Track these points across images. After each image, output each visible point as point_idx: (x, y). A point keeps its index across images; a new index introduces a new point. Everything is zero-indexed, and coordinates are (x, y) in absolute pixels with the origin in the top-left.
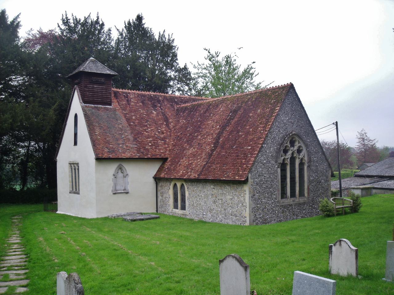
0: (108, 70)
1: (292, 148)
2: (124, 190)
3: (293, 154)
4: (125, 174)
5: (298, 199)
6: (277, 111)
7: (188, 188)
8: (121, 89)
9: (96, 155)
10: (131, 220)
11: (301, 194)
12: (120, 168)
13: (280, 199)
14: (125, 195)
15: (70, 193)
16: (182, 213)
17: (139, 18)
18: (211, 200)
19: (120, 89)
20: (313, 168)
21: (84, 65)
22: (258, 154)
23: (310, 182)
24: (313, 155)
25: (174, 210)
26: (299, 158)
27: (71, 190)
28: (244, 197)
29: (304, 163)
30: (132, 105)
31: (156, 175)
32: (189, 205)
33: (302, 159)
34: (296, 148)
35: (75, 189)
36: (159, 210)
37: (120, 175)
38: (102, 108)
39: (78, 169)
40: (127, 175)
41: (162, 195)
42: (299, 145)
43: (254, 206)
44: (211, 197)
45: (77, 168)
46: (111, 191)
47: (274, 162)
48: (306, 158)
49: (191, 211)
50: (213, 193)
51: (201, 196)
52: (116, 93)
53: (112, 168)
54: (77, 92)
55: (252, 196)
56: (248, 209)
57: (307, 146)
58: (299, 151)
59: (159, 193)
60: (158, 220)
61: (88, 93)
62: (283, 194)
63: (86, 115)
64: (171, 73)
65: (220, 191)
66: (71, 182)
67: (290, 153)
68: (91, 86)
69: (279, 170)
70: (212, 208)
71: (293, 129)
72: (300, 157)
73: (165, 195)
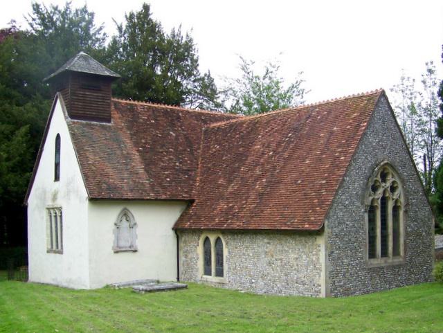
0: (106, 70)
1: (383, 184)
2: (130, 247)
3: (384, 192)
4: (132, 223)
5: (391, 260)
6: (364, 128)
7: (227, 244)
9: (90, 193)
10: (146, 291)
11: (396, 252)
12: (125, 214)
13: (368, 259)
14: (130, 255)
15: (48, 252)
16: (218, 281)
17: (146, 8)
18: (264, 260)
20: (411, 214)
21: (72, 62)
22: (337, 191)
23: (407, 234)
24: (411, 195)
25: (205, 277)
26: (393, 199)
27: (50, 247)
28: (316, 254)
29: (400, 206)
30: (140, 123)
31: (176, 224)
32: (229, 268)
33: (397, 201)
34: (388, 184)
35: (56, 247)
36: (182, 277)
37: (125, 224)
38: (97, 125)
39: (61, 216)
40: (135, 224)
41: (186, 255)
42: (393, 179)
43: (331, 268)
44: (263, 256)
45: (58, 214)
47: (359, 204)
48: (402, 200)
49: (232, 277)
50: (267, 250)
51: (249, 255)
52: (115, 103)
53: (111, 215)
54: (61, 102)
55: (330, 255)
56: (323, 274)
57: (403, 181)
58: (393, 189)
59: (181, 254)
60: (184, 291)
61: (76, 103)
62: (372, 255)
63: (74, 136)
64: (187, 84)
65: (279, 247)
66: (50, 236)
67: (380, 191)
69: (366, 216)
70: (265, 272)
71: (384, 157)
72: (394, 197)
73: (190, 256)
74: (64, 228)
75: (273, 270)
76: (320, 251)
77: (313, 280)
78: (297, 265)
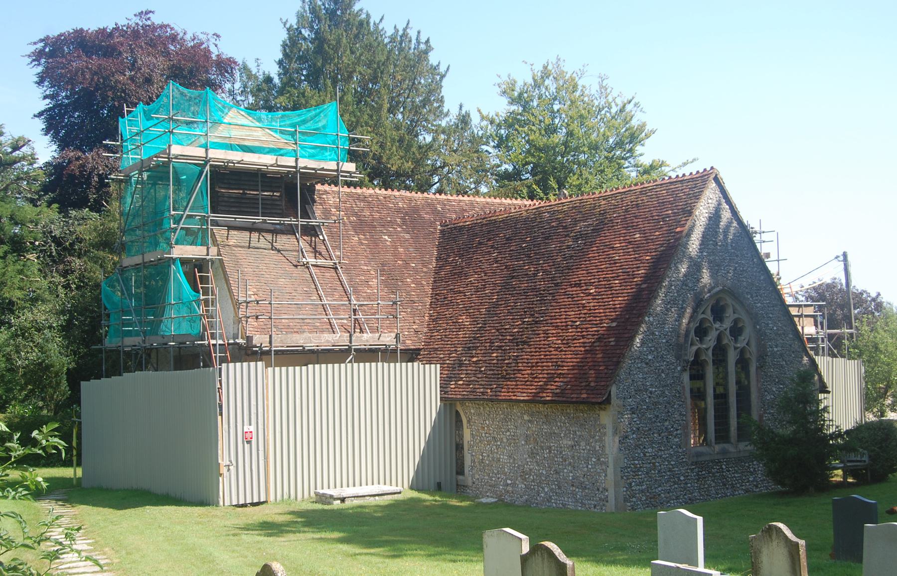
3: (719, 338)
24: (771, 340)
26: (736, 348)
32: (473, 461)
33: (742, 351)
34: (727, 324)
42: (736, 316)
48: (753, 348)
56: (610, 471)
74: (183, 154)
75: (538, 465)
76: (605, 434)
77: (597, 481)
78: (573, 457)
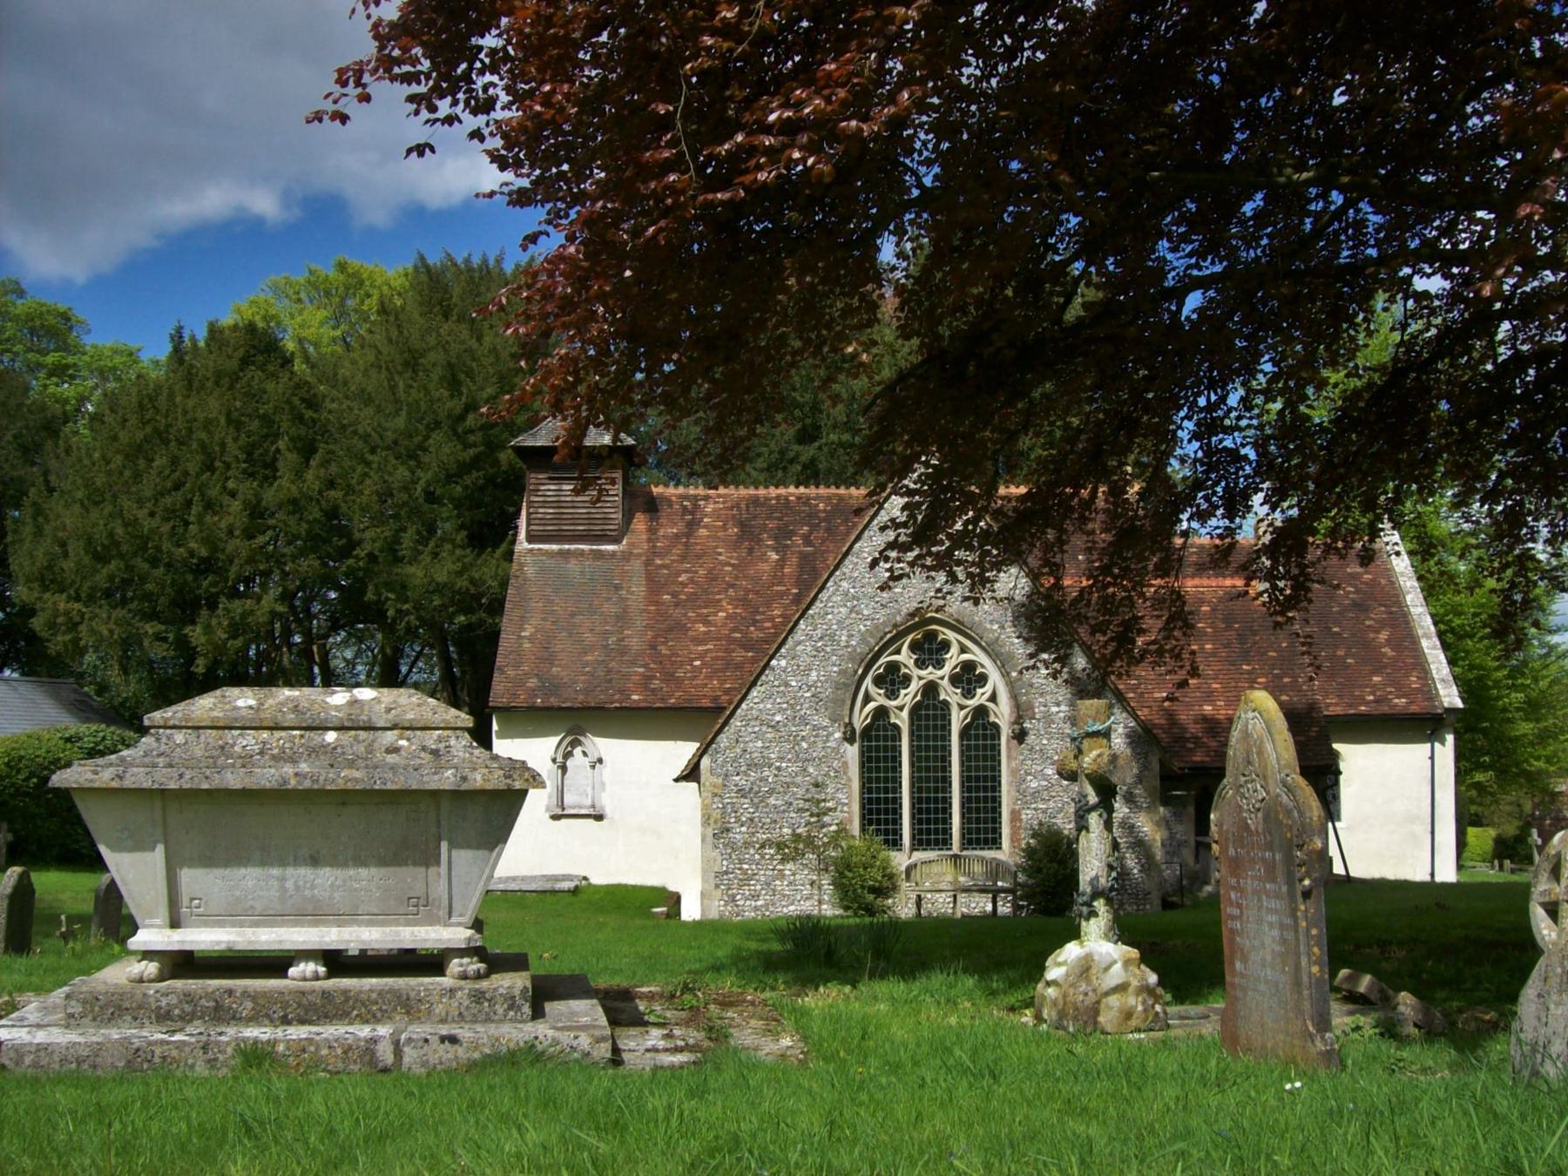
8: (843, 487)
19: (786, 487)
33: (981, 712)
46: (544, 809)
68: (552, 487)
